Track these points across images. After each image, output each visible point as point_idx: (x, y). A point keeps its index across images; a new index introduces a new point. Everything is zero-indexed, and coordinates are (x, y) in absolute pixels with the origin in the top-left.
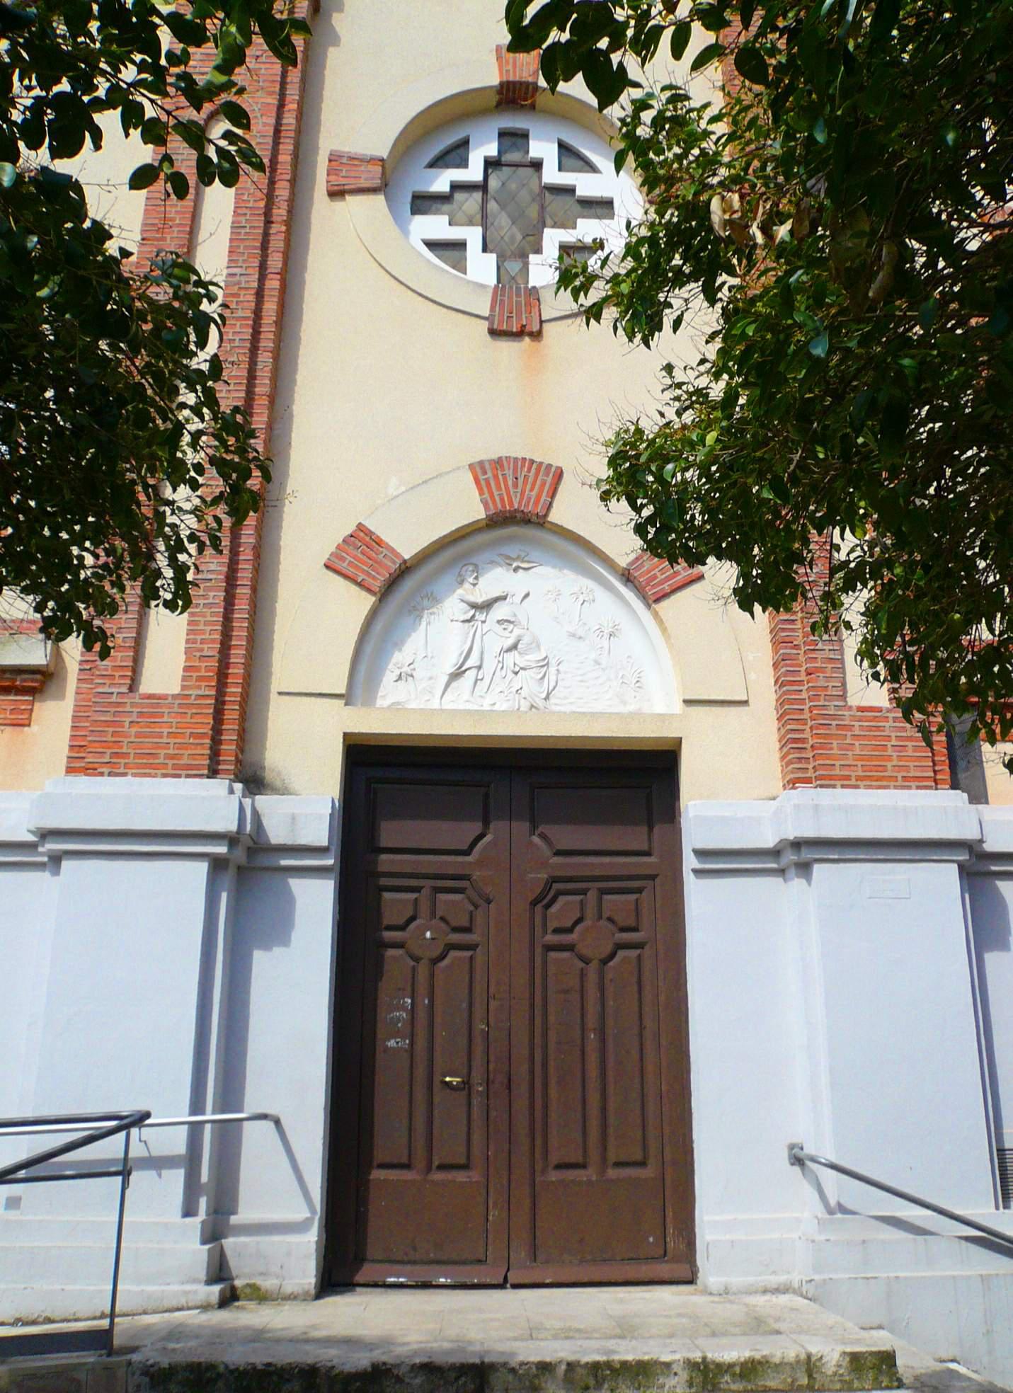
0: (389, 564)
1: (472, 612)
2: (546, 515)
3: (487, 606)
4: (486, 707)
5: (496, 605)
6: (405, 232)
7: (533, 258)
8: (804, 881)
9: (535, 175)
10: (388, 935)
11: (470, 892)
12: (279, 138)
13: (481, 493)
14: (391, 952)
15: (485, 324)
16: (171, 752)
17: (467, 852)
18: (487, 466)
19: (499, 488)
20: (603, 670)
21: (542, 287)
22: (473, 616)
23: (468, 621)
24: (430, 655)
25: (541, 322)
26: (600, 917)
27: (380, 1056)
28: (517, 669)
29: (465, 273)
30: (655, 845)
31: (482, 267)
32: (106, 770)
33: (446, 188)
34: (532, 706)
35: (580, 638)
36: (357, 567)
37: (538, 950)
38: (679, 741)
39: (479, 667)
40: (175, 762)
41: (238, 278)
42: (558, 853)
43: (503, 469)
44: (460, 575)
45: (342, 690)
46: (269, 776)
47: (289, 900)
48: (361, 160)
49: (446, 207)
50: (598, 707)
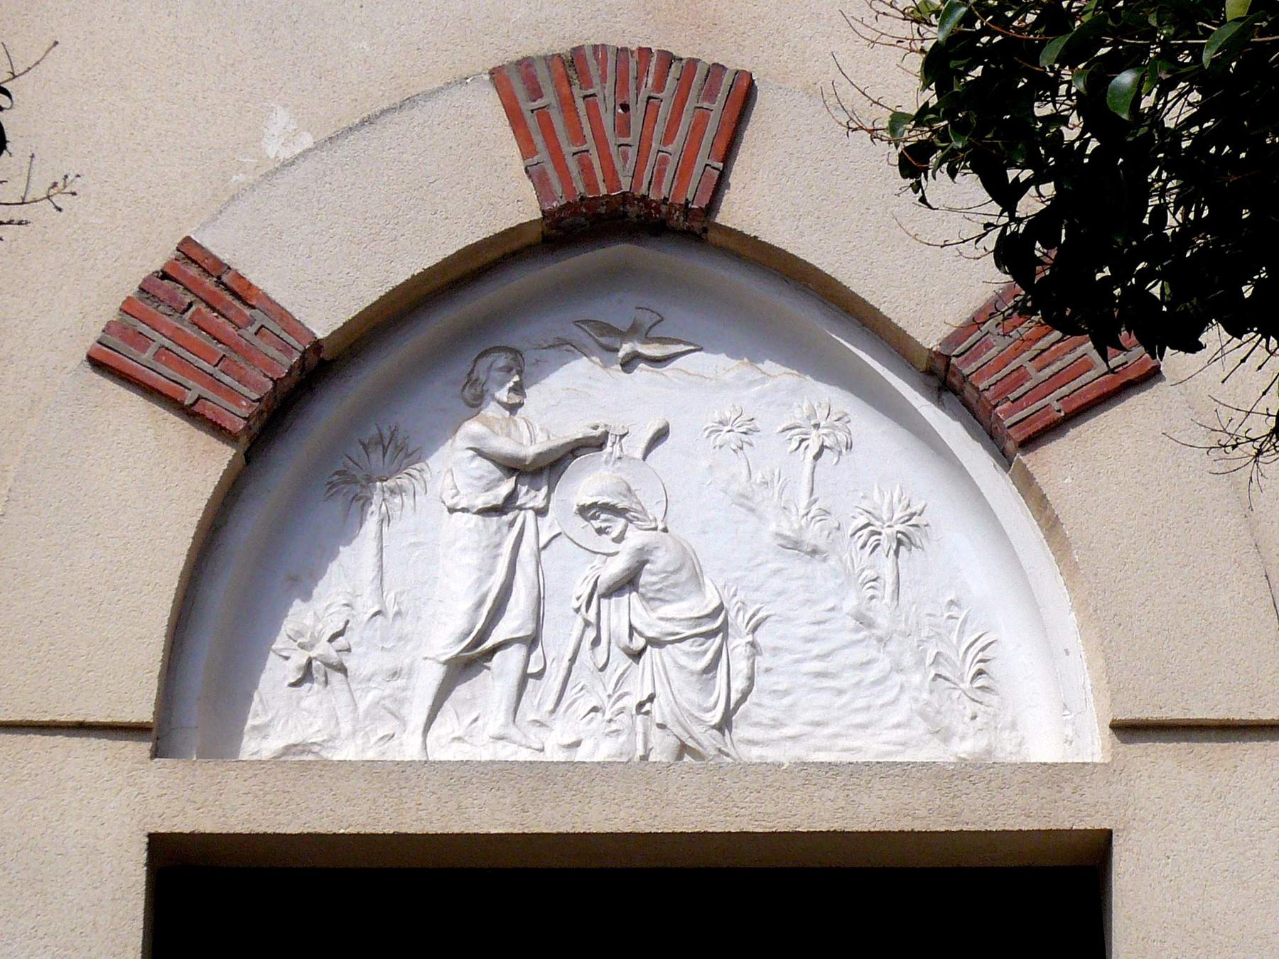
13: (527, 148)
18: (542, 75)
19: (578, 136)
22: (512, 496)
28: (639, 643)
34: (683, 749)
36: (182, 364)
39: (532, 642)
44: (471, 381)
45: (144, 712)
50: (872, 747)
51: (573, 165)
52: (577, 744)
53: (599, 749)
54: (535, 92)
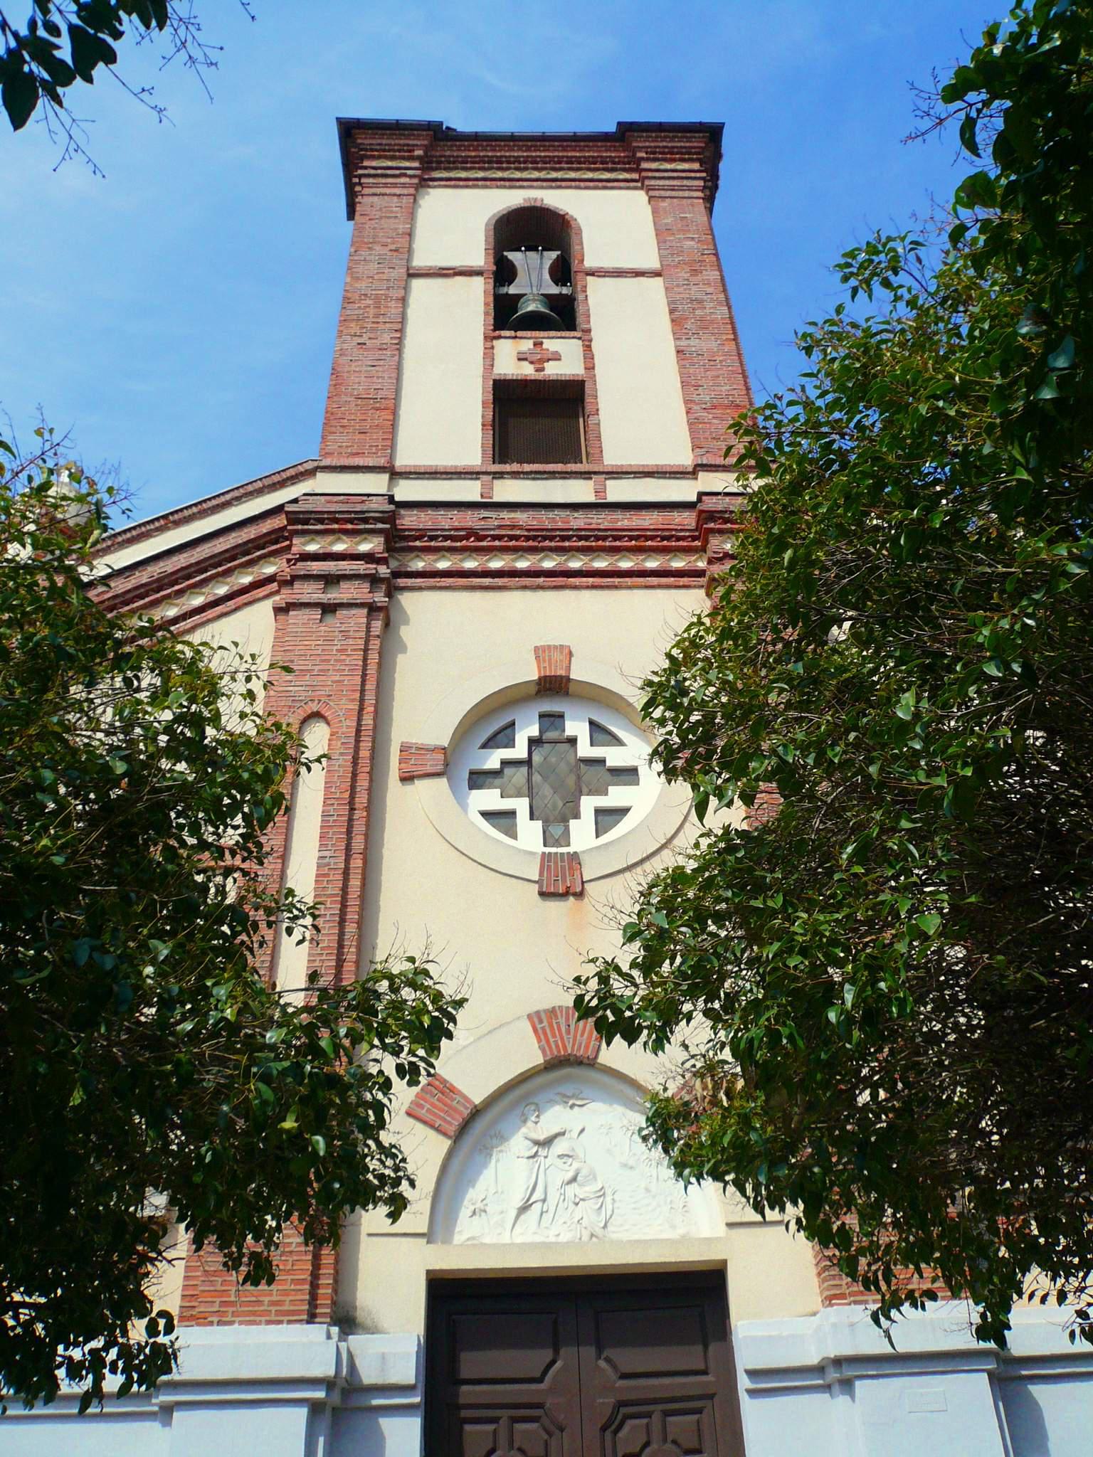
0: (462, 1109)
1: (535, 1149)
2: (596, 1057)
3: (547, 1143)
4: (553, 1239)
5: (556, 1141)
6: (463, 806)
7: (573, 823)
8: (847, 1398)
9: (572, 750)
11: (546, 1421)
12: (360, 736)
13: (539, 1040)
15: (536, 887)
16: (275, 1298)
17: (540, 1380)
18: (543, 1016)
19: (554, 1036)
20: (654, 1197)
21: (584, 852)
22: (537, 1152)
23: (533, 1157)
24: (500, 1191)
25: (583, 883)
26: (665, 1440)
28: (577, 1200)
29: (515, 837)
30: (712, 1364)
31: (530, 833)
32: (215, 1319)
33: (497, 766)
34: (592, 1235)
35: (631, 1168)
36: (435, 1115)
38: (725, 1262)
39: (544, 1201)
40: (278, 1308)
41: (327, 860)
42: (624, 1376)
43: (557, 1018)
44: (523, 1114)
45: (424, 1230)
46: (360, 1315)
48: (427, 750)
49: (497, 781)
50: (650, 1234)
51: (554, 1047)
52: (558, 1235)
53: (564, 1238)
54: (541, 1021)
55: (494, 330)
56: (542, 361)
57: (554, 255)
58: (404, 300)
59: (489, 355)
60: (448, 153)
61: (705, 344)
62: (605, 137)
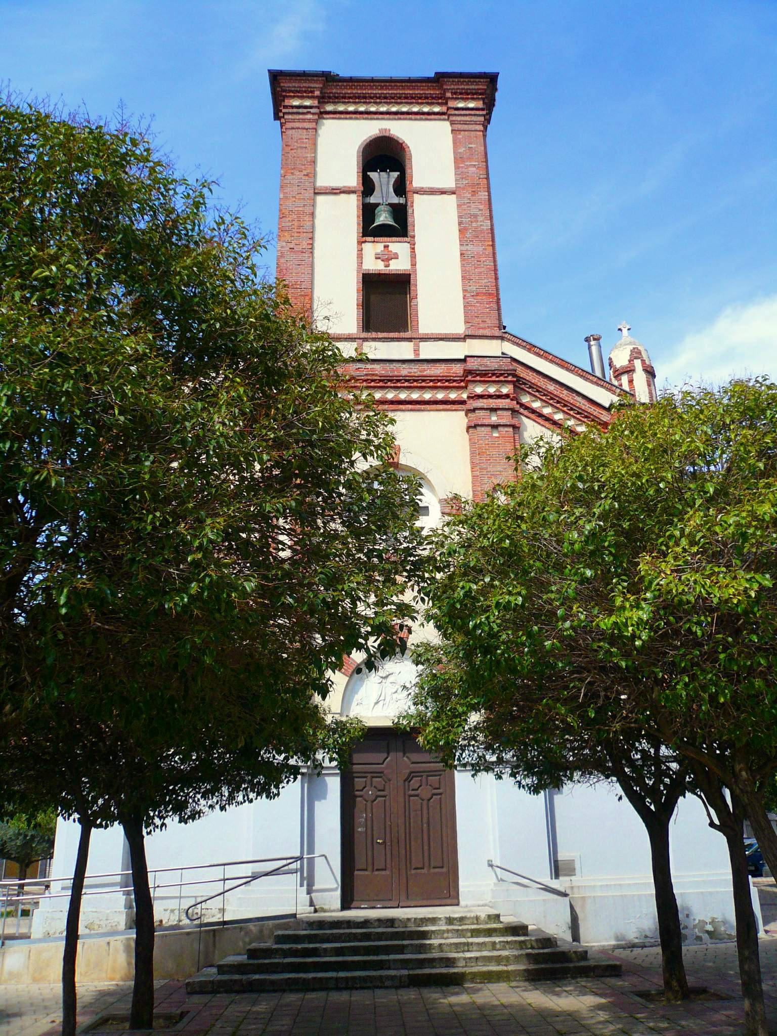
10: (357, 793)
14: (358, 799)
27: (356, 835)
37: (407, 797)
47: (325, 785)
55: (363, 236)
56: (388, 260)
57: (395, 174)
58: (314, 206)
59: (360, 256)
60: (334, 91)
61: (474, 249)
62: (428, 80)
